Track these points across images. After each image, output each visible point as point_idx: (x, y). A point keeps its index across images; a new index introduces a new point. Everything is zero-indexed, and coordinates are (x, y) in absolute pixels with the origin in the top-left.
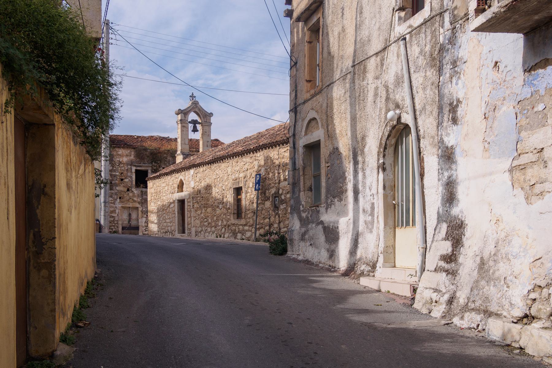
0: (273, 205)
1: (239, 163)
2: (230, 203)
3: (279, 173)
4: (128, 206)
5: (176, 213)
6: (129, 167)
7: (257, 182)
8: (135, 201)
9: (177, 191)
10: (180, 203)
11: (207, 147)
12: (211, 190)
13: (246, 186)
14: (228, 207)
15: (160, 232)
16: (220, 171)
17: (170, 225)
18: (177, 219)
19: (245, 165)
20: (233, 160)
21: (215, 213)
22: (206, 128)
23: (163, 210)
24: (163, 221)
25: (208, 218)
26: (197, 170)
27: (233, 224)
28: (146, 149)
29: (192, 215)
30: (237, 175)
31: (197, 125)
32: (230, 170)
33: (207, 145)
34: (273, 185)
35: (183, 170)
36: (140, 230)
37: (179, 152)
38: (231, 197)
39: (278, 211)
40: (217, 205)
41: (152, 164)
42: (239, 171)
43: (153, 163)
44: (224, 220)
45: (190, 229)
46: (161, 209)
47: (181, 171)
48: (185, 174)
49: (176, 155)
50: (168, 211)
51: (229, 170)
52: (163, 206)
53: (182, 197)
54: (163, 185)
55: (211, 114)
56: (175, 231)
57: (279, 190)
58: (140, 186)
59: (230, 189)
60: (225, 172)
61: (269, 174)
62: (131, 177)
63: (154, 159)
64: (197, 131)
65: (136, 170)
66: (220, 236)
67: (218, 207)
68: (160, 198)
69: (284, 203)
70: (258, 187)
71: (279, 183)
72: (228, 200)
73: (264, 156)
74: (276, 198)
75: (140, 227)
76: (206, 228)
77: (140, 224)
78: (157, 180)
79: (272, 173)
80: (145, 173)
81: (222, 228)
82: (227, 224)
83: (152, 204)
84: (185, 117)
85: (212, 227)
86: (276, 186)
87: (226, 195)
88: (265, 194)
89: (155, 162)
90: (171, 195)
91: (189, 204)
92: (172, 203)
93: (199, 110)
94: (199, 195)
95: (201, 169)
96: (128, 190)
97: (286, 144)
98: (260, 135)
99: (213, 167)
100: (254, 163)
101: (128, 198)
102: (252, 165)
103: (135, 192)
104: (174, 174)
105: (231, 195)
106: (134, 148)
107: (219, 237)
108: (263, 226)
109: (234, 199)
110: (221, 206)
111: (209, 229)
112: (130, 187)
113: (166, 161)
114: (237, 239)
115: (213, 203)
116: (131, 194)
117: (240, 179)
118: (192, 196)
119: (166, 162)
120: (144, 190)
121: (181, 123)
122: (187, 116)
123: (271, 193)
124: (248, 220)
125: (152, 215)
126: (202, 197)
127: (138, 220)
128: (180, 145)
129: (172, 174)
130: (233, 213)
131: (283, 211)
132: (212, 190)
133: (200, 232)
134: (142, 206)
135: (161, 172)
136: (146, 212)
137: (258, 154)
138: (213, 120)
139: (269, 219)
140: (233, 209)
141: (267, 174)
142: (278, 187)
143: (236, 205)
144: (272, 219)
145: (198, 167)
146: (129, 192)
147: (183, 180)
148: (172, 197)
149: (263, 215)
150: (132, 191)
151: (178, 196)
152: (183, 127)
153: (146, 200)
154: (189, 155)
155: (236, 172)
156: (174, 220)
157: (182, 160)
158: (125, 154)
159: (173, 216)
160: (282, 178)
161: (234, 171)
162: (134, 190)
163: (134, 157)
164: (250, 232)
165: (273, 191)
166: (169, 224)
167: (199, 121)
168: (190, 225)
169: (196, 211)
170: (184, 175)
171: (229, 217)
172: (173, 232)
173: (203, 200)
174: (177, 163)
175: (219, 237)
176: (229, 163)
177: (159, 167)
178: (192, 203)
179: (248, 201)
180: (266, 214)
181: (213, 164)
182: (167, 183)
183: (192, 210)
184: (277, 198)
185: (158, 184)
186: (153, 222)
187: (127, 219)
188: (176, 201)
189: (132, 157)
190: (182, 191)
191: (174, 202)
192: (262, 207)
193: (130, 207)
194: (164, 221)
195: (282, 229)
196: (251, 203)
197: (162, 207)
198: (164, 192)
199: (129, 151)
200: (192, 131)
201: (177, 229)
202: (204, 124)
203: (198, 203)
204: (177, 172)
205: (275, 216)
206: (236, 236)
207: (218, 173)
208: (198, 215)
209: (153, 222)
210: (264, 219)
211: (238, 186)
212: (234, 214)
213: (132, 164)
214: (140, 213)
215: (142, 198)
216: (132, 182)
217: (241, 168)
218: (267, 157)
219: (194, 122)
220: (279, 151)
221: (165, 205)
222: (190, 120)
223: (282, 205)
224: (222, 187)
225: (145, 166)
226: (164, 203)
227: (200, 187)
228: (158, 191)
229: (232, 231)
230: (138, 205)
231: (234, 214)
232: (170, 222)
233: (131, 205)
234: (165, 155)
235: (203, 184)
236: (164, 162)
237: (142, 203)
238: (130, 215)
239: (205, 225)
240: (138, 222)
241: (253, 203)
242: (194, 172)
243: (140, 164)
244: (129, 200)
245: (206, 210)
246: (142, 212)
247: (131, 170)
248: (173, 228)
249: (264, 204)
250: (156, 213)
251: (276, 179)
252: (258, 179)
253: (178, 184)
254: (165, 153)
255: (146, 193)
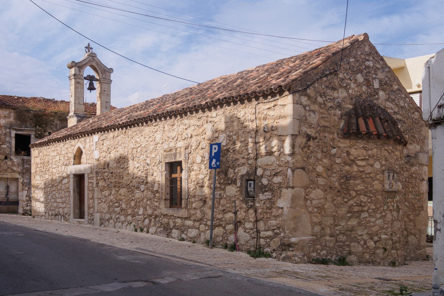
0: (244, 193)
1: (176, 126)
2: (159, 184)
3: (256, 143)
4: (5, 176)
5: (72, 191)
6: (8, 130)
7: (213, 155)
8: (14, 171)
9: (72, 162)
10: (77, 178)
11: (106, 108)
12: (126, 164)
13: (190, 161)
14: (155, 189)
15: (47, 214)
16: (143, 137)
17: (62, 206)
18: (72, 199)
19: (186, 129)
20: (165, 122)
21: (133, 196)
22: (105, 86)
23: (53, 186)
24: (52, 200)
25: (121, 202)
26: (104, 136)
27: (164, 215)
28: (28, 111)
29: (95, 196)
30: (172, 145)
31: (93, 82)
32: (160, 136)
33: (106, 106)
34: (243, 161)
35: (82, 136)
36: (20, 205)
37: (71, 114)
38: (162, 175)
39: (254, 203)
40: (136, 185)
41: (36, 127)
42: (176, 138)
43: (37, 127)
44: (148, 207)
45: (92, 215)
46: (49, 184)
47: (79, 136)
48: (85, 141)
49: (68, 117)
50: (59, 188)
51: (158, 136)
52: (52, 180)
53: (80, 170)
54: (53, 154)
55: (111, 70)
56: (69, 215)
57: (256, 169)
58: (20, 153)
59: (159, 164)
60: (151, 139)
61: (234, 143)
62: (10, 143)
63: (39, 122)
64: (94, 89)
65: (17, 136)
66: (142, 230)
67: (138, 188)
68: (49, 170)
69: (267, 191)
70: (216, 163)
71: (256, 159)
72: (155, 179)
73: (226, 117)
74: (249, 182)
75: (20, 202)
76: (118, 216)
77: (20, 198)
78: (45, 148)
79: (241, 142)
80: (27, 138)
81: (145, 218)
82: (152, 213)
83: (38, 177)
84: (80, 71)
85: (126, 215)
86: (250, 162)
87: (151, 171)
88: (226, 174)
89: (40, 126)
90: (63, 167)
91: (90, 181)
92: (66, 178)
93: (97, 64)
94: (106, 170)
95: (111, 134)
96: (6, 158)
97: (272, 97)
98: (163, 100)
99: (130, 132)
100: (205, 126)
101: (5, 167)
102: (201, 130)
103: (14, 160)
104: (68, 140)
105: (162, 172)
106: (14, 109)
107: (139, 230)
108: (221, 223)
109: (166, 179)
110: (142, 187)
111: (122, 218)
112: (8, 155)
113: (52, 125)
114: (172, 237)
115: (129, 182)
116: (9, 163)
117: (179, 149)
118: (96, 170)
119: (52, 126)
120: (26, 158)
121: (75, 78)
122: (82, 71)
123: (240, 174)
124: (192, 212)
125: (37, 191)
126: (112, 173)
127: (18, 193)
128: (73, 105)
129: (66, 141)
130: (164, 198)
131: (264, 203)
132: (128, 164)
133: (108, 220)
134: (23, 177)
135: (50, 137)
136: (28, 185)
137: (214, 113)
138: (113, 76)
139: (235, 213)
140: (164, 193)
141: (231, 143)
142: (253, 165)
143: (169, 187)
144: (241, 215)
145: (106, 132)
146: (7, 160)
147: (82, 148)
148: (66, 170)
149: (223, 206)
150: (11, 159)
151: (74, 169)
152: (77, 83)
153: (29, 171)
154: (85, 117)
155: (171, 140)
156: (68, 199)
157: (75, 124)
158: (3, 116)
159: (67, 195)
160: (263, 150)
161: (166, 138)
162: (13, 157)
163: (14, 119)
164: (197, 231)
165: (243, 170)
166: (61, 205)
167: (97, 77)
168: (92, 209)
169: (102, 191)
170: (83, 142)
171: (157, 204)
172: (67, 216)
173: (112, 176)
174: (69, 126)
175: (139, 230)
176: (157, 127)
177: (45, 131)
178: (95, 180)
179: (193, 184)
180: (228, 205)
181: (130, 127)
182: (59, 151)
183: (96, 189)
184: (252, 182)
185: (45, 153)
186: (38, 200)
187: (3, 192)
188: (72, 176)
189: (12, 119)
190: (80, 163)
191: (68, 176)
192: (220, 195)
193: (7, 178)
194: (54, 200)
195: (262, 233)
196: (198, 187)
197: (50, 181)
198: (53, 163)
199: (8, 112)
200: (88, 89)
201: (72, 212)
202: (102, 82)
203: (105, 181)
204: (39, 146)
205: (248, 210)
206: (171, 232)
207: (138, 140)
208: (105, 196)
209: (38, 200)
210: (225, 213)
211: (173, 160)
212: (166, 200)
213: (11, 127)
214: (20, 185)
215: (23, 168)
216: (11, 148)
217: (180, 133)
218: (231, 117)
219: (91, 79)
220: (257, 108)
221: (56, 179)
222: (85, 75)
223: (263, 193)
224: (145, 160)
225: (27, 130)
226: (54, 178)
227: (108, 159)
228: (46, 161)
229: (161, 225)
230: (17, 176)
231: (166, 200)
232: (63, 203)
233: (9, 176)
234: (52, 118)
235: (113, 155)
236: (51, 126)
237: (23, 173)
238: (8, 187)
239: (116, 211)
240: (18, 196)
241: (202, 187)
242: (99, 139)
243: (22, 127)
244: (6, 170)
245: (118, 191)
246: (23, 183)
247: (10, 134)
248: (66, 210)
249: (224, 189)
250: (42, 189)
251: (250, 152)
252: (214, 151)
253: (75, 152)
254: (51, 116)
255: (29, 162)
